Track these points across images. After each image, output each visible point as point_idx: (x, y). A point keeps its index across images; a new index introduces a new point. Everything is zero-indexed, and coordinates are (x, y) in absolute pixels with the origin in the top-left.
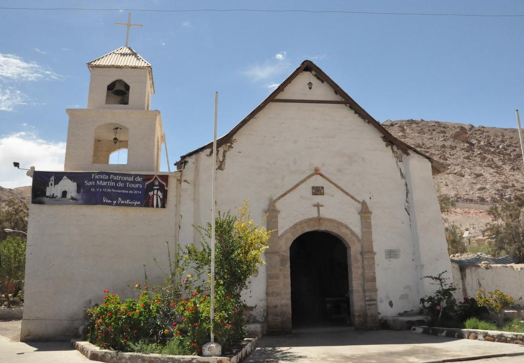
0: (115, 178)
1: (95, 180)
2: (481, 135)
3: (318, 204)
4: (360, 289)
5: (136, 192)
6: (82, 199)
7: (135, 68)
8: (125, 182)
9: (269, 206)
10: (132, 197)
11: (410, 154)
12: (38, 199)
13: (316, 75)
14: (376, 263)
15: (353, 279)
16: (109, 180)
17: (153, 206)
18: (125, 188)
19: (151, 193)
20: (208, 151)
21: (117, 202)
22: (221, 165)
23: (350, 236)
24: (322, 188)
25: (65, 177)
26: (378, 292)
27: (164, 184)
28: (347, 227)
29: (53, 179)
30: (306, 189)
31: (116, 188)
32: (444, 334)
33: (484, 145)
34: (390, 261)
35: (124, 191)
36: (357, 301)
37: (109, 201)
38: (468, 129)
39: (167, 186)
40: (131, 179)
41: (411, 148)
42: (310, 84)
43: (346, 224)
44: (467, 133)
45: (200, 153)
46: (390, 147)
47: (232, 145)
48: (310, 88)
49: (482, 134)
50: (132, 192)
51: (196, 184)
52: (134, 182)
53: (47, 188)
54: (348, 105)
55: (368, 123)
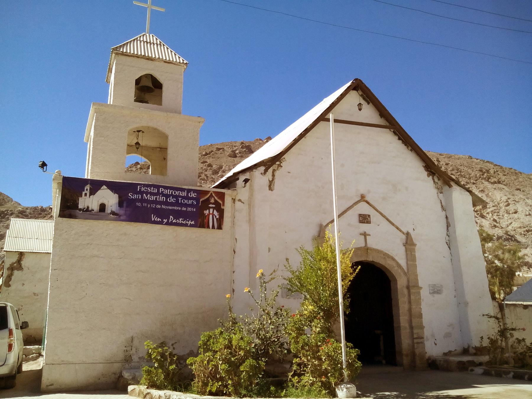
0: (166, 192)
1: (141, 193)
3: (365, 232)
4: (407, 325)
5: (189, 209)
7: (169, 62)
8: (176, 197)
10: (186, 216)
11: (452, 186)
12: (67, 212)
13: (361, 96)
14: (422, 298)
15: (400, 315)
17: (208, 227)
18: (177, 204)
19: (206, 212)
20: (262, 169)
23: (396, 268)
24: (369, 216)
25: (104, 187)
26: (425, 330)
28: (393, 259)
29: (89, 189)
30: (352, 216)
31: (166, 203)
32: (512, 374)
34: (434, 296)
35: (176, 208)
36: (405, 340)
37: (159, 219)
39: (224, 205)
40: (184, 194)
41: (453, 180)
43: (392, 255)
45: (254, 170)
46: (431, 177)
48: (360, 110)
50: (185, 209)
51: (250, 205)
53: (80, 198)
54: (392, 130)
55: (411, 150)
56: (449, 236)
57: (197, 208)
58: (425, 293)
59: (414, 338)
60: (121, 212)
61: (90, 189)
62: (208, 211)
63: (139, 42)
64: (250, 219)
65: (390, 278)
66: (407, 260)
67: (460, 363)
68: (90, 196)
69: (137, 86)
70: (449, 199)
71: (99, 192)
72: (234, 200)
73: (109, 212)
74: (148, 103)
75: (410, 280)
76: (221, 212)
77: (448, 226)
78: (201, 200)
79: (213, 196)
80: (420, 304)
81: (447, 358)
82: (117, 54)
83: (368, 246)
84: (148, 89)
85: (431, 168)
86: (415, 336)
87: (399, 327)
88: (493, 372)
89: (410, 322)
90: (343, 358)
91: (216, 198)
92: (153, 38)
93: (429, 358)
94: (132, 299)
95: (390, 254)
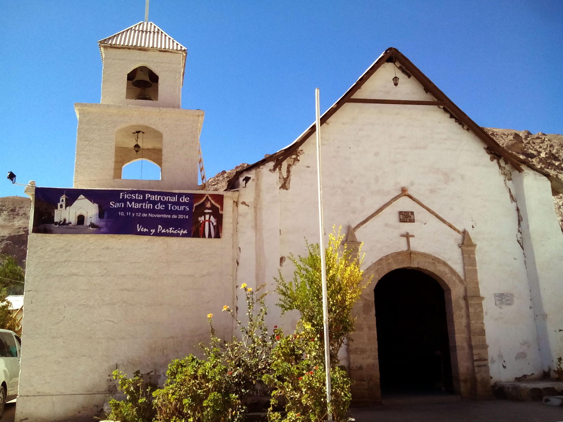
0: (153, 198)
1: (124, 200)
2: (541, 145)
3: (407, 233)
4: (465, 345)
5: (181, 216)
8: (166, 203)
10: (178, 224)
11: (523, 170)
12: (42, 227)
13: (400, 68)
14: (484, 310)
15: (456, 332)
16: (144, 201)
17: (204, 236)
18: (166, 211)
19: (201, 219)
20: (271, 164)
22: (285, 183)
23: (449, 275)
25: (82, 196)
26: (489, 349)
28: (445, 264)
30: (390, 215)
31: (153, 211)
33: (546, 157)
34: (501, 308)
35: (165, 216)
36: (463, 364)
37: (145, 230)
38: (523, 137)
39: (222, 209)
40: (175, 199)
42: (396, 79)
43: (443, 259)
44: (523, 142)
45: (261, 167)
46: (495, 161)
47: (298, 158)
48: (396, 84)
49: (542, 143)
51: (257, 207)
52: (178, 203)
53: (56, 211)
54: (442, 107)
55: (468, 130)
56: (521, 233)
57: (188, 214)
58: (489, 305)
59: (474, 361)
60: (102, 224)
61: (66, 199)
62: (203, 217)
63: (133, 31)
64: (256, 225)
65: (443, 288)
66: (464, 265)
67: (534, 390)
68: (66, 207)
69: (131, 82)
70: (520, 186)
71: (76, 203)
72: (236, 203)
73: (88, 224)
74: (152, 100)
75: (468, 289)
76: (219, 218)
77: (520, 220)
78: (195, 205)
79: (209, 200)
80: (482, 318)
81: (518, 384)
82: (105, 47)
83: (412, 249)
84: (143, 84)
85: (494, 150)
86: (475, 358)
87: (455, 347)
89: (469, 340)
90: (327, 390)
91: (213, 201)
92: (151, 26)
93: (496, 384)
94: (115, 321)
95: (440, 258)
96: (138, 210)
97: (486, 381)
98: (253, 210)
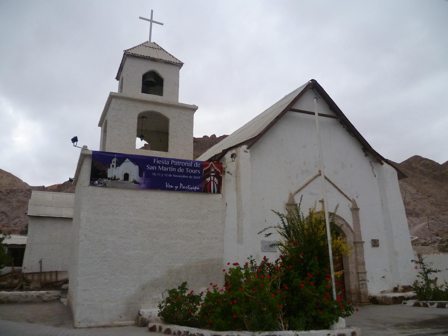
1: (157, 165)
4: (354, 271)
5: (195, 177)
6: (144, 183)
9: (290, 198)
16: (170, 165)
18: (185, 173)
19: (208, 179)
21: (179, 187)
25: (127, 160)
26: (367, 274)
27: (220, 171)
28: (343, 220)
31: (177, 173)
35: (184, 176)
37: (171, 186)
53: (109, 169)
54: (339, 120)
55: (353, 136)
61: (117, 162)
64: (237, 188)
78: (204, 170)
79: (213, 166)
81: (384, 295)
86: (360, 279)
88: (421, 304)
96: (166, 172)
97: (366, 294)
98: (235, 178)
